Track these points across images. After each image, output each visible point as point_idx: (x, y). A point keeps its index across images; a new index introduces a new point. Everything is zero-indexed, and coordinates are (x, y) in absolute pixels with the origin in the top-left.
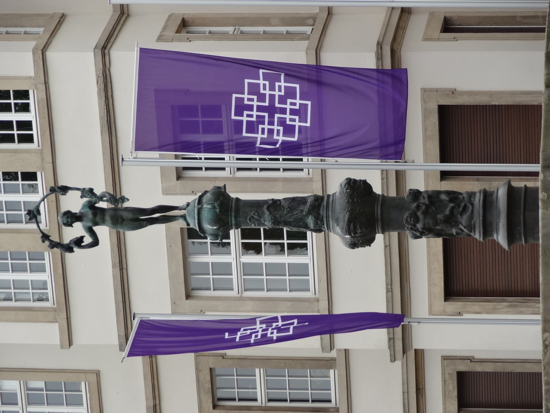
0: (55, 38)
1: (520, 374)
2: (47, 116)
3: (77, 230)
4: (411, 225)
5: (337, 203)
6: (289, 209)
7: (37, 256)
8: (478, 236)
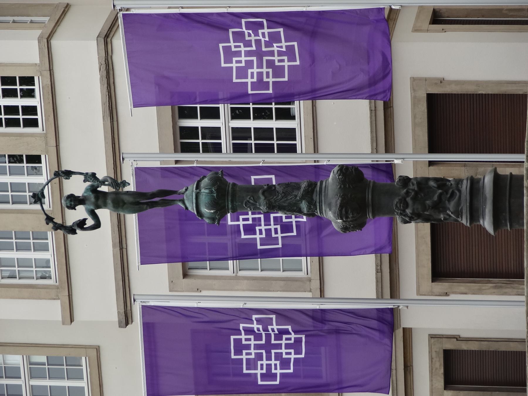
0: (59, 27)
1: (505, 353)
2: (51, 102)
3: (80, 213)
4: (401, 210)
5: (329, 188)
6: (283, 194)
7: (41, 236)
8: (465, 221)
